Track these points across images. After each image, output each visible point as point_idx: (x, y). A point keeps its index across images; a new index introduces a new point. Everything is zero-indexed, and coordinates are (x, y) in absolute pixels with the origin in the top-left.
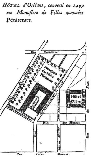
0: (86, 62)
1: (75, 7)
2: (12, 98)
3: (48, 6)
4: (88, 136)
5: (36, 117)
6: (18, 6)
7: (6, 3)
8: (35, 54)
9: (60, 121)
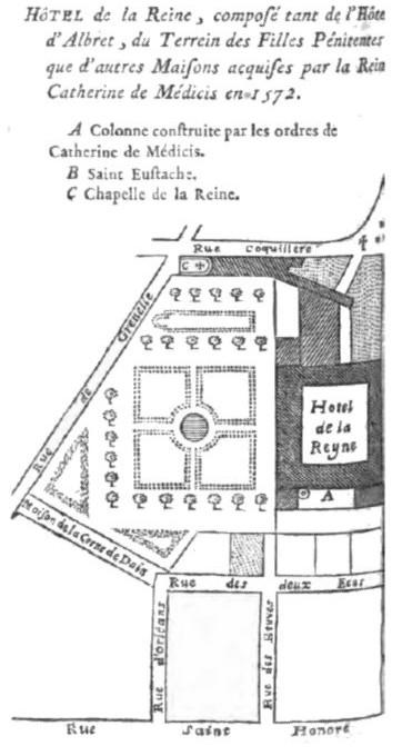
1: (285, 62)
2: (203, 313)
3: (216, 19)
5: (374, 240)
6: (76, 20)
7: (38, 9)
8: (197, 237)
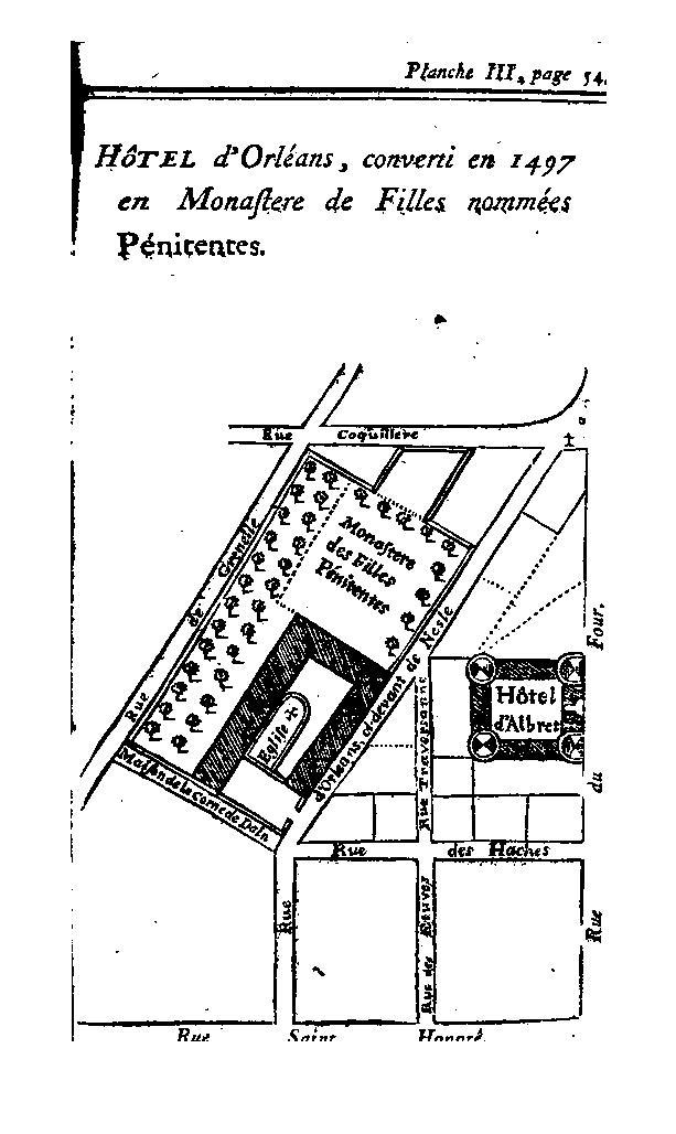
0: (586, 493)
3: (365, 164)
4: (596, 929)
6: (184, 165)
9: (433, 842)
